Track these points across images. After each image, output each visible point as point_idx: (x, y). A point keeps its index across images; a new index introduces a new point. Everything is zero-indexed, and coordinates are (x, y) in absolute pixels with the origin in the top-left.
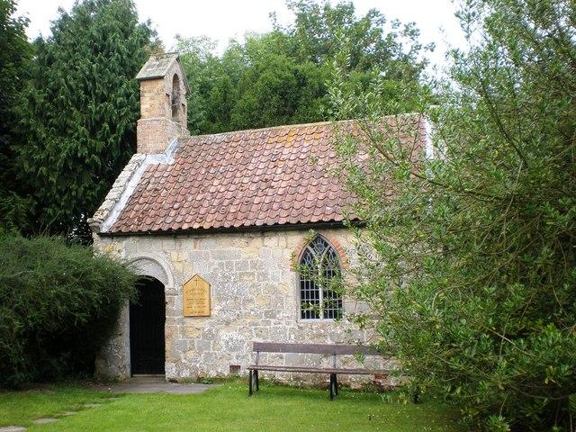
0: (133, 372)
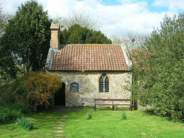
0: (56, 104)
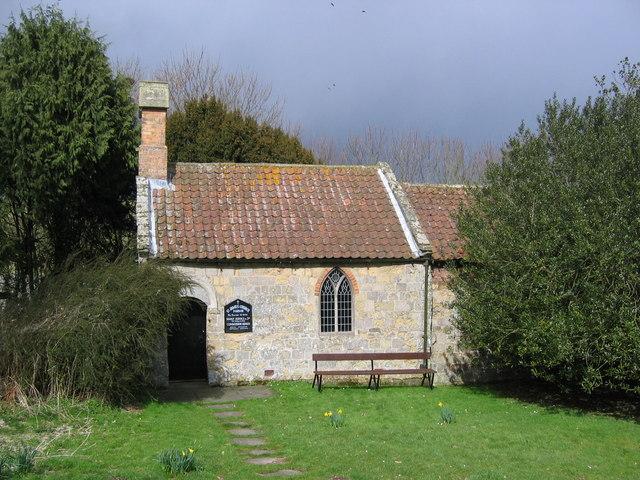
0: (173, 376)
